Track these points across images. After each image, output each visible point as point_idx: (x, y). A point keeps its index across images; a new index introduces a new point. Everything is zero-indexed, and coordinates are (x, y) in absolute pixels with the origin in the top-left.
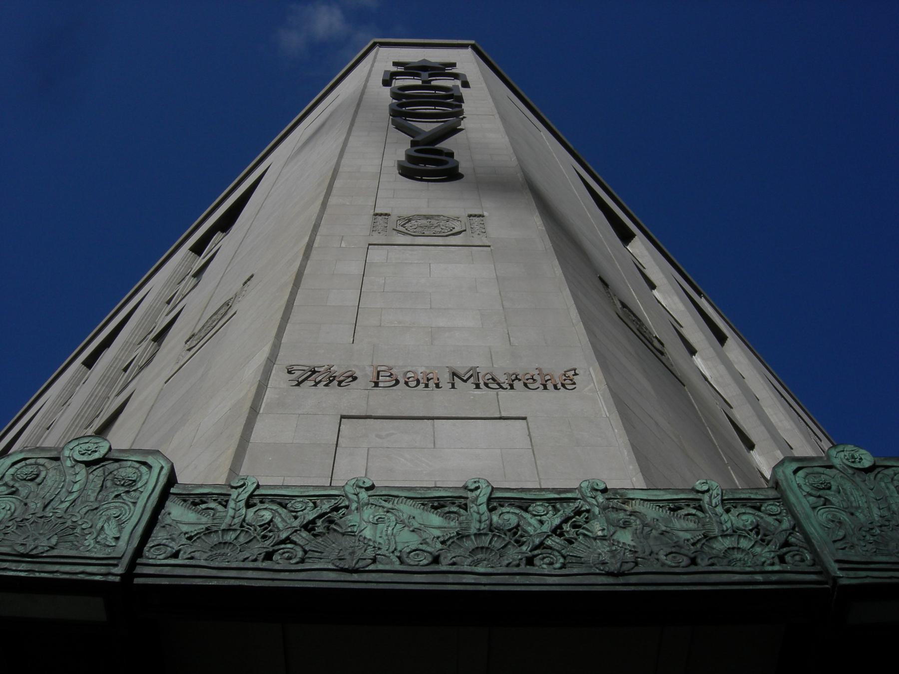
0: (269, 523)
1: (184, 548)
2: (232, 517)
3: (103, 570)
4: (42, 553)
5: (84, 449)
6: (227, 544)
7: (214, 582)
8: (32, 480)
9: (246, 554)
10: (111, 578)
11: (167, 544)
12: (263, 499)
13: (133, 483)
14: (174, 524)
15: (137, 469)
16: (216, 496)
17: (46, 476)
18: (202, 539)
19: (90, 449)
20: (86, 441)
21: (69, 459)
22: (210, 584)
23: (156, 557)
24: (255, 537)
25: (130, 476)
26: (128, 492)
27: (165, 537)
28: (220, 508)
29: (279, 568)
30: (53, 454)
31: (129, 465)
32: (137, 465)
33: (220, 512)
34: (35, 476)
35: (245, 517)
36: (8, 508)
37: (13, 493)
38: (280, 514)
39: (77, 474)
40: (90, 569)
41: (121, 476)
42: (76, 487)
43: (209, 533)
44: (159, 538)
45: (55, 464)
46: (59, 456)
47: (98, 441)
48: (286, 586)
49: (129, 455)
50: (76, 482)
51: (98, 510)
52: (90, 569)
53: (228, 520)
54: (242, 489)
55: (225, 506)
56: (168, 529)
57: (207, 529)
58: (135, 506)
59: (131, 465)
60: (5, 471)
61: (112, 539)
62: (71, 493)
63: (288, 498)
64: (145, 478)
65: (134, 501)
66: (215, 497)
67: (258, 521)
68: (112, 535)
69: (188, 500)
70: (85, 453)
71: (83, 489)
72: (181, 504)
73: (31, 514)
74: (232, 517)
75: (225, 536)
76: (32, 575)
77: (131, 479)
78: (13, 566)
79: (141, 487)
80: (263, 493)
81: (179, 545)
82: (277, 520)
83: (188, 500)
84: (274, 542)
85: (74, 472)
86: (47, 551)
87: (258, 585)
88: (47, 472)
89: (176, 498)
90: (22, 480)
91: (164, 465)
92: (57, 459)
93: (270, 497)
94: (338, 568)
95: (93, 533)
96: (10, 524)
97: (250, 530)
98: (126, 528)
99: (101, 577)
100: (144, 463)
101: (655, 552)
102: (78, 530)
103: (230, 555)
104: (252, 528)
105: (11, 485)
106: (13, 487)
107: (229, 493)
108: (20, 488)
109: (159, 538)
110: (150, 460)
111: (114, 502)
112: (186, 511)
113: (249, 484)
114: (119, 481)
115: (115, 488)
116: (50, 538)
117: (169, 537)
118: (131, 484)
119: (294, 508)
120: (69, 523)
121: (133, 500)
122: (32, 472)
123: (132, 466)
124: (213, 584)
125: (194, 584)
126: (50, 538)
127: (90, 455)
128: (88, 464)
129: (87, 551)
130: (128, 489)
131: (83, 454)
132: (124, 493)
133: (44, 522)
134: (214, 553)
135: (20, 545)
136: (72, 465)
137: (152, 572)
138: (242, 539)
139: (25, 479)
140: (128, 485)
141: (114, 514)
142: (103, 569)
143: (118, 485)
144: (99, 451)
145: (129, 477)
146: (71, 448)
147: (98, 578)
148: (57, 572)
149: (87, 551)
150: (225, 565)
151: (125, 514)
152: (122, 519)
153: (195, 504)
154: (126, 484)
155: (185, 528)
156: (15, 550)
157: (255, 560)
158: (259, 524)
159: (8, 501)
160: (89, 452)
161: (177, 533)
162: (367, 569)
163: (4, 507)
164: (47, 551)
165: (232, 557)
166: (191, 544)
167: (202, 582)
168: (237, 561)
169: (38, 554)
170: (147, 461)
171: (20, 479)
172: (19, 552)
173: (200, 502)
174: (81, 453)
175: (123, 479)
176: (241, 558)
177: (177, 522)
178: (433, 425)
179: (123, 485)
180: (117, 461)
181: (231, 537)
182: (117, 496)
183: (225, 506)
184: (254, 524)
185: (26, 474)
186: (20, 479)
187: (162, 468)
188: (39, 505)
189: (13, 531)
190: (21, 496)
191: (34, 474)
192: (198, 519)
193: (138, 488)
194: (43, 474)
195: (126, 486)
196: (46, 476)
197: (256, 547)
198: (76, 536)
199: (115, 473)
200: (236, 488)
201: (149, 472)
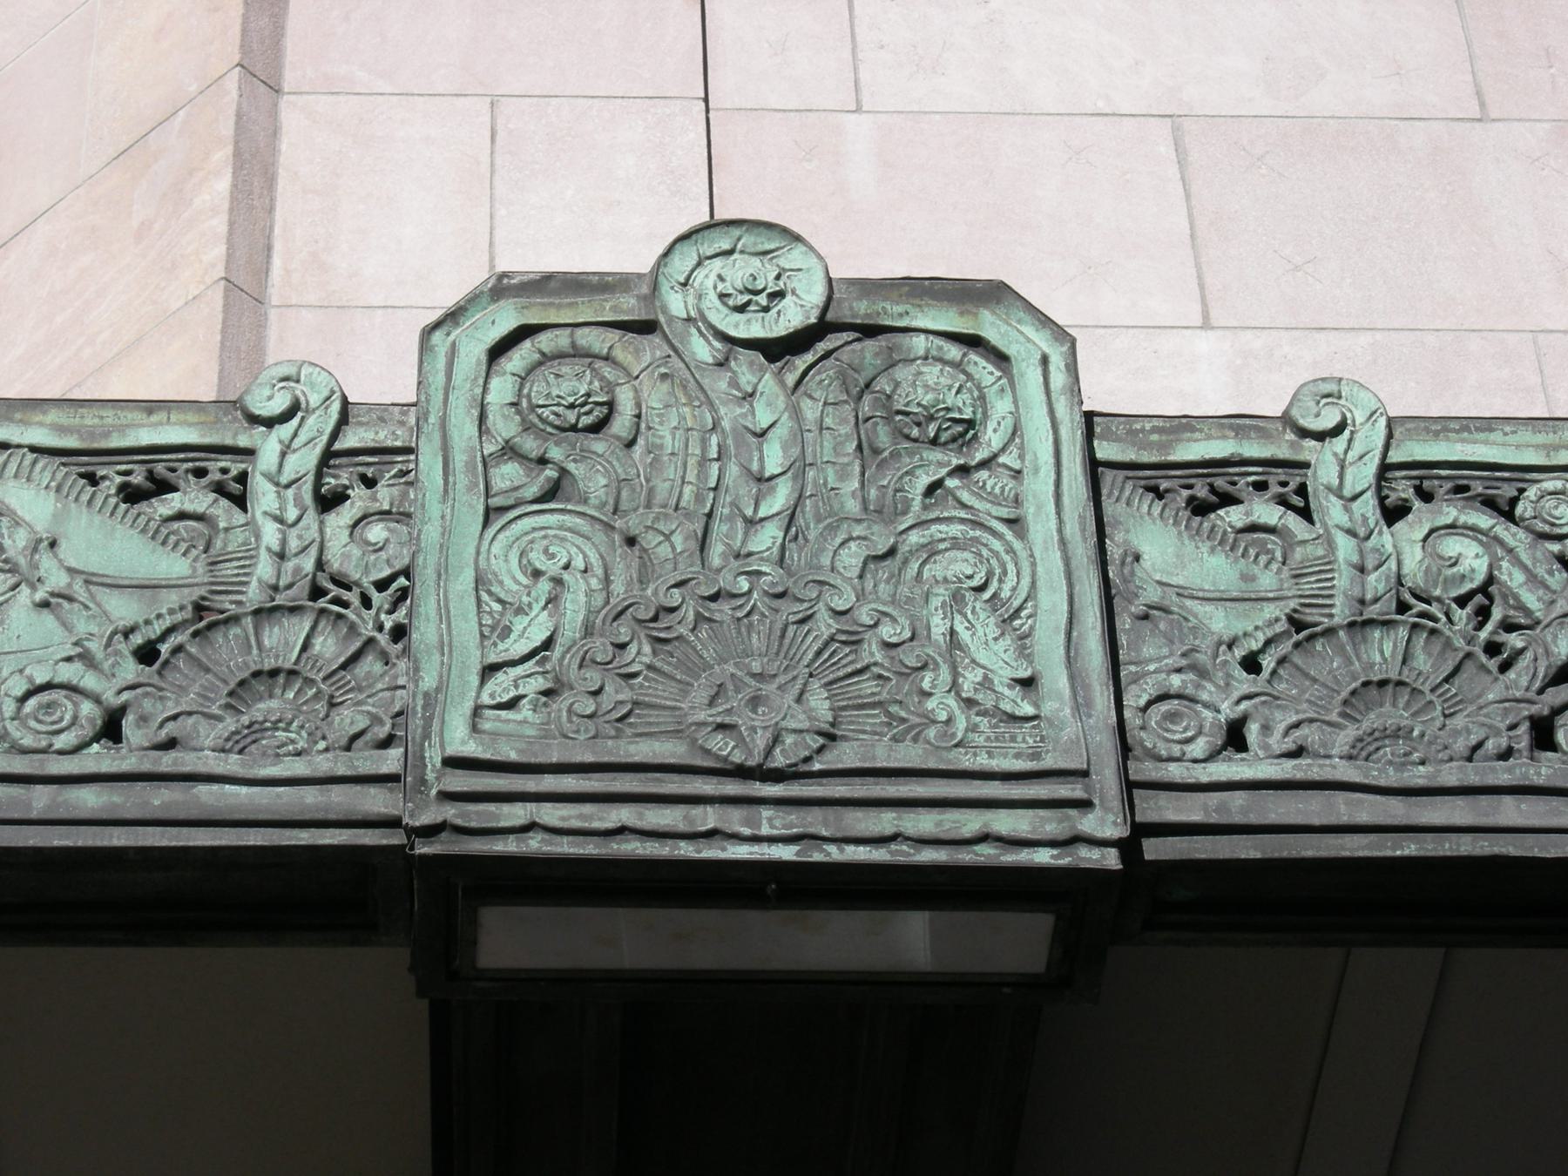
0: (1484, 589)
1: (1255, 706)
2: (1355, 567)
3: (1050, 824)
4: (807, 760)
5: (739, 286)
6: (1390, 688)
7: (1410, 848)
8: (597, 428)
9: (348, 719)
10: (1089, 857)
11: (1190, 691)
12: (1421, 478)
13: (967, 431)
14: (1173, 600)
15: (957, 365)
16: (1260, 469)
17: (638, 405)
18: (189, 655)
19: (760, 285)
20: (726, 246)
21: (694, 331)
22: (1398, 853)
23: (51, 745)
24: (1468, 655)
25: (949, 403)
26: (963, 471)
27: (1169, 661)
28: (223, 511)
29: (1357, 780)
30: (628, 307)
31: (921, 353)
32: (954, 351)
33: (1304, 542)
34: (605, 410)
35: (1399, 563)
36: (579, 563)
37: (551, 493)
38: (1510, 551)
39: (752, 395)
40: (1005, 822)
41: (919, 404)
42: (774, 458)
43: (212, 626)
44: (1152, 667)
45: (651, 348)
46: (652, 317)
47: (772, 246)
48: (1309, 853)
49: (908, 307)
50: (762, 434)
51: (899, 557)
52: (1005, 822)
53: (265, 569)
54: (295, 422)
55: (240, 501)
56: (1162, 626)
57: (200, 609)
58: (1022, 535)
59: (928, 350)
60: (479, 391)
61: (1010, 687)
62: (763, 481)
63: (1506, 475)
64: (1001, 407)
65: (1012, 516)
66: (1255, 474)
67: (1449, 582)
68: (1008, 673)
69: (103, 478)
70: (749, 303)
71: (798, 468)
72: (85, 497)
73: (676, 585)
74: (1355, 567)
75: (267, 633)
76: (817, 857)
77: (957, 416)
78: (735, 820)
79: (1003, 450)
80: (1419, 458)
81: (1236, 695)
82: (1511, 577)
83: (103, 478)
84: (1541, 675)
85: (739, 389)
86: (820, 750)
87: (164, 842)
88: (636, 391)
89: (64, 470)
90: (563, 430)
91: (1047, 350)
92: (646, 327)
93: (1443, 473)
94: (728, 767)
95: (936, 664)
96: (623, 632)
97: (345, 605)
98: (1037, 634)
99: (1055, 852)
100: (973, 342)
101: (1240, 633)
102: (872, 652)
103: (1422, 735)
104: (353, 597)
105: (534, 455)
106: (543, 461)
107: (1301, 457)
108: (571, 467)
109: (1152, 667)
110: (990, 326)
111: (938, 520)
112: (1189, 546)
113: (1359, 420)
114: (918, 424)
115: (911, 454)
116: (802, 693)
117: (1184, 662)
118: (962, 435)
119: (1545, 521)
120: (825, 625)
121: (1004, 512)
122: (588, 395)
123: (934, 353)
124: (1406, 852)
125: (1346, 854)
126: (802, 693)
127: (766, 309)
128: (776, 350)
129: (956, 746)
130: (962, 462)
131: (741, 309)
132: (951, 474)
133: (739, 619)
134: (245, 720)
135: (715, 730)
136: (720, 357)
137: (1196, 817)
138: (328, 646)
139: (574, 428)
140: (954, 440)
141: (970, 577)
142: (1049, 820)
143: (915, 440)
144: (793, 292)
145: (948, 409)
146: (682, 280)
147: (1043, 857)
148: (621, 830)
149: (956, 746)
150: (1419, 776)
151: (1005, 573)
152: (1006, 593)
153: (131, 495)
154: (944, 437)
155: (1219, 622)
156: (707, 752)
157: (1506, 754)
158: (1454, 594)
159: (561, 528)
160: (763, 300)
161: (1206, 645)
162: (817, 766)
163: (564, 560)
164: (820, 750)
165: (1430, 743)
166: (156, 680)
167: (1367, 847)
168: (1451, 759)
169: (795, 765)
170: (983, 334)
171: (557, 427)
172: (718, 757)
173: (149, 485)
174: (731, 303)
175: (931, 418)
176: (1461, 745)
177: (90, 580)
178: (717, 109)
179: (934, 442)
180: (870, 331)
181: (1382, 652)
182: (931, 489)
183: (240, 501)
184: (1437, 592)
185: (572, 406)
186: (557, 427)
187: (1045, 360)
188: (677, 539)
189: (650, 667)
190: (593, 501)
191: (597, 404)
192: (1247, 578)
193: (995, 456)
194: (625, 399)
195: (946, 443)
196: (638, 405)
197: (1491, 697)
198: (880, 677)
199: (883, 384)
200: (270, 423)
201: (1004, 381)
